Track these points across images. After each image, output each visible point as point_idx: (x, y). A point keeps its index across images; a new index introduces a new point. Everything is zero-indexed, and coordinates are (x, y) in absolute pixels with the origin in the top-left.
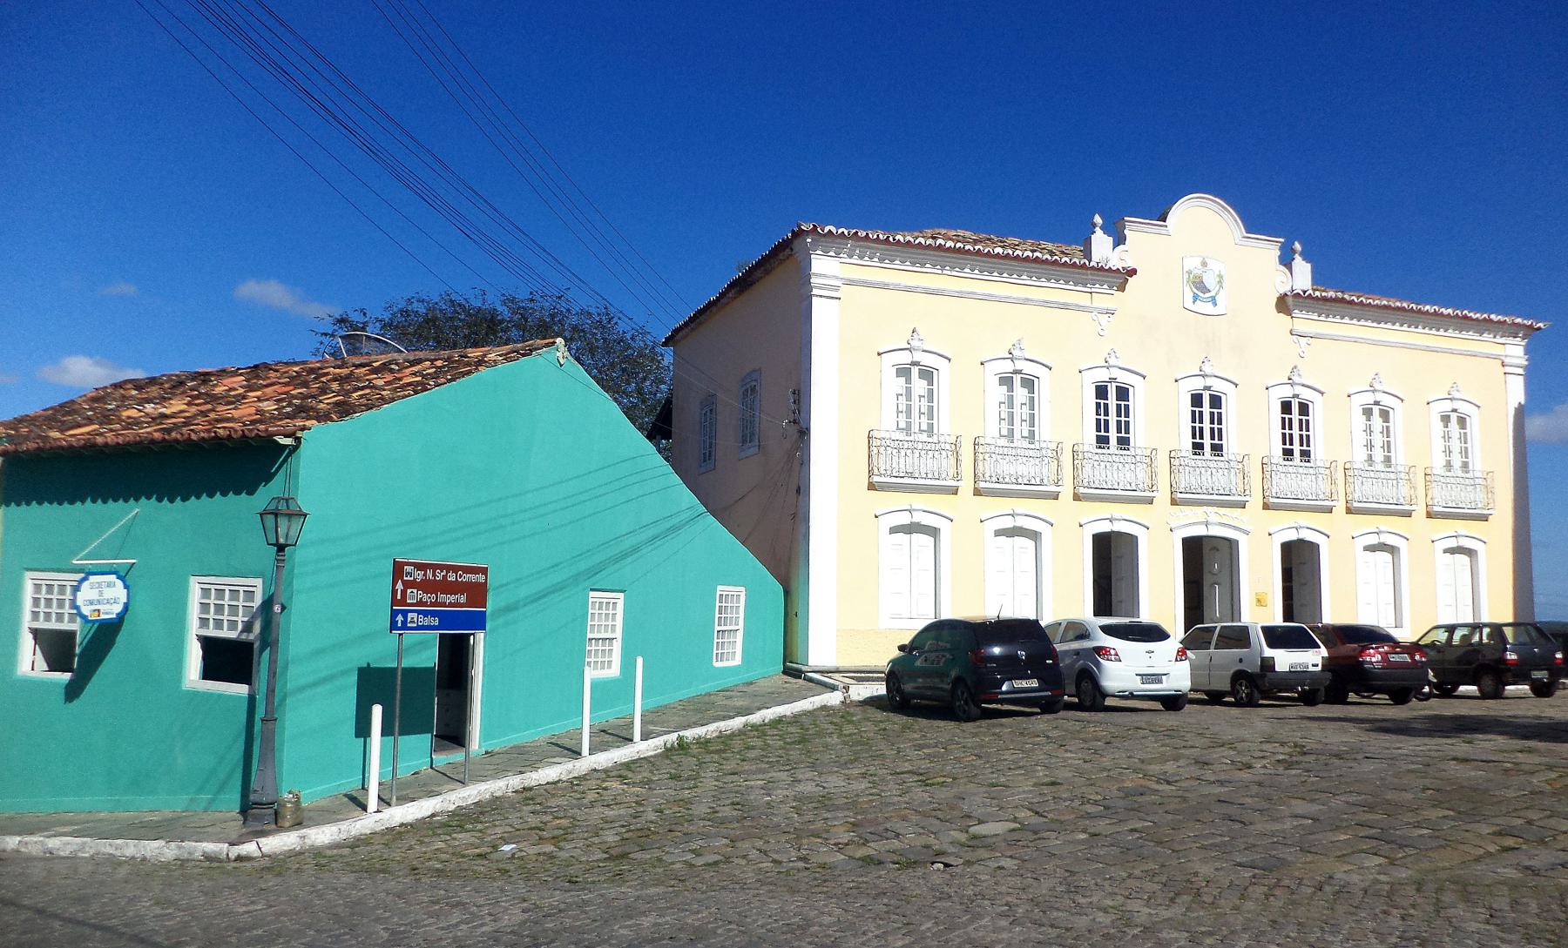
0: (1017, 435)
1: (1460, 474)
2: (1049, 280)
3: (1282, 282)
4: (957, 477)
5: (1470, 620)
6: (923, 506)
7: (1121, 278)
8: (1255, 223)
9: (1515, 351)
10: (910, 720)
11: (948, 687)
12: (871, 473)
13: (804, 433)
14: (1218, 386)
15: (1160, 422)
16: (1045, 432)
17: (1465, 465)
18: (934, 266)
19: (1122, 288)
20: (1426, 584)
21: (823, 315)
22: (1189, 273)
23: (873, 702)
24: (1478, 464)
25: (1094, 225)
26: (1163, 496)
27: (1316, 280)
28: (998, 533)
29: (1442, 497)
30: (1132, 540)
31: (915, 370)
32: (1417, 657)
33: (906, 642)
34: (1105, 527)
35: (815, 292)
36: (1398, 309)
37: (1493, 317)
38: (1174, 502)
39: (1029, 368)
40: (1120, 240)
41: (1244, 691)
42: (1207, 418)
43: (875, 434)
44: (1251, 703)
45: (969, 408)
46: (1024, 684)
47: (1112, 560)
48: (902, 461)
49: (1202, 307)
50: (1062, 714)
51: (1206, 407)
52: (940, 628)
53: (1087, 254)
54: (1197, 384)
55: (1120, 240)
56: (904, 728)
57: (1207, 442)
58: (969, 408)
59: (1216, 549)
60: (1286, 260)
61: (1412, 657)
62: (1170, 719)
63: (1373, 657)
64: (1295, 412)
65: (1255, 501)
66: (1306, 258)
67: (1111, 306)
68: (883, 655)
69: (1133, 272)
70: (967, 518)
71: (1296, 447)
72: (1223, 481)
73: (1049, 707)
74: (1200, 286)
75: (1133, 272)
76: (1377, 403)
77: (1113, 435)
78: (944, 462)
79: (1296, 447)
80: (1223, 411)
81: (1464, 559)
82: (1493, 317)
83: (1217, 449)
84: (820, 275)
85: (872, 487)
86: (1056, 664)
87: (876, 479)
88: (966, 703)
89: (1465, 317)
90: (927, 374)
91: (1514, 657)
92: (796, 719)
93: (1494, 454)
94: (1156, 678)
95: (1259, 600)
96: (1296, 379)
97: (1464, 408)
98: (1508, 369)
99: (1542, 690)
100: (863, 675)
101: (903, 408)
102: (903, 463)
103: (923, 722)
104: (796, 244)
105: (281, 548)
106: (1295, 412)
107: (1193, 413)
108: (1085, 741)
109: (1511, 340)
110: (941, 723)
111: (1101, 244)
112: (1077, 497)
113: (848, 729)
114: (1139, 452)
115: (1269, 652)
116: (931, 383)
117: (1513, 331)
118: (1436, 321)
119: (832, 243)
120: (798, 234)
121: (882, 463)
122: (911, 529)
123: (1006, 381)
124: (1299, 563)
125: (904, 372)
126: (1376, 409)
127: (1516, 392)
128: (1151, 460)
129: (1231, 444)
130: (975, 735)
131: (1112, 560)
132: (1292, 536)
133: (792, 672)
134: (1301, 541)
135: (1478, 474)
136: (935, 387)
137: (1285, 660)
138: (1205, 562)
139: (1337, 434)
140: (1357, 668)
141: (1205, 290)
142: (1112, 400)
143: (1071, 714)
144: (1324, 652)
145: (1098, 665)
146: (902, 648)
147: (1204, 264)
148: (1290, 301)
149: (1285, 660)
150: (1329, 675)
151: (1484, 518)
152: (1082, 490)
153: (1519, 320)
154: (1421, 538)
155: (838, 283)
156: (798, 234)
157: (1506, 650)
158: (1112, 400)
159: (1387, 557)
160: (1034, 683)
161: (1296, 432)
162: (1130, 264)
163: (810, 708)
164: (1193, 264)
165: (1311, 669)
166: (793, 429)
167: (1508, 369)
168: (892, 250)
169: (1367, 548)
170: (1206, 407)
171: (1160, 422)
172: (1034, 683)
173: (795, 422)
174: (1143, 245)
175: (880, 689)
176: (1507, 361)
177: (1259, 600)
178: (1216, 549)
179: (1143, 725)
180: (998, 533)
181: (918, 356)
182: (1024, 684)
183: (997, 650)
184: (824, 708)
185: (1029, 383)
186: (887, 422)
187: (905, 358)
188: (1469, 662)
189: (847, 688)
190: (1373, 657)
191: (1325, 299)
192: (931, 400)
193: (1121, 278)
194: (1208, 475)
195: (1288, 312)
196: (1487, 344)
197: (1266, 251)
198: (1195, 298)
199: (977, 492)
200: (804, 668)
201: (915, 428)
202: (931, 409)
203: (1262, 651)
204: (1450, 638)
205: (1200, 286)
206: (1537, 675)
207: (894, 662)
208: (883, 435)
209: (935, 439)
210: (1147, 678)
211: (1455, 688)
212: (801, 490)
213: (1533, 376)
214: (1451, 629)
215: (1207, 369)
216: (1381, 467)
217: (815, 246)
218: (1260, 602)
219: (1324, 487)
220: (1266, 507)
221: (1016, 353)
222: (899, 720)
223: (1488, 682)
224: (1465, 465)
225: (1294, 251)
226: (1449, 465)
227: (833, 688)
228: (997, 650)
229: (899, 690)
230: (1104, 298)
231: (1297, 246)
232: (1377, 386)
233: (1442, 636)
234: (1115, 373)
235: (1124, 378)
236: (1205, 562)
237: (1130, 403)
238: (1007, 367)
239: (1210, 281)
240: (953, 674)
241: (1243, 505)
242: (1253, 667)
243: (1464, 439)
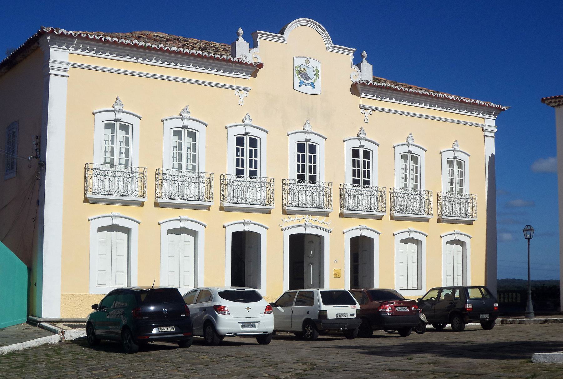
0: (184, 168)
1: (457, 196)
2: (207, 69)
3: (354, 75)
4: (144, 195)
5: (460, 285)
6: (120, 215)
7: (254, 69)
8: (339, 38)
9: (490, 122)
10: (94, 351)
11: (120, 331)
12: (86, 192)
13: (42, 164)
14: (314, 139)
15: (277, 163)
16: (203, 167)
17: (461, 191)
18: (132, 57)
19: (254, 75)
20: (431, 261)
21: (58, 90)
22: (298, 67)
23: (79, 341)
24: (468, 190)
25: (238, 35)
26: (277, 208)
27: (375, 72)
28: (170, 231)
29: (450, 209)
30: (256, 237)
31: (117, 125)
32: (413, 308)
33: (98, 303)
34: (240, 228)
35: (52, 72)
36: (423, 94)
37: (477, 101)
38: (284, 212)
39: (192, 125)
40: (254, 45)
41: (309, 331)
42: (247, 153)
43: (89, 166)
44: (313, 339)
45: (151, 150)
46: (166, 329)
47: (244, 248)
48: (107, 184)
49: (304, 88)
50: (192, 347)
51: (306, 151)
52: (117, 294)
53: (233, 54)
54: (301, 138)
55: (254, 45)
56: (91, 357)
57: (247, 169)
58: (151, 150)
59: (312, 242)
60: (357, 62)
61: (410, 309)
62: (263, 348)
63: (388, 309)
64: (361, 156)
65: (335, 211)
66: (369, 61)
67: (247, 86)
68: (85, 312)
69: (261, 66)
70: (149, 222)
71: (361, 176)
72: (316, 199)
73: (183, 343)
74: (303, 74)
75: (261, 66)
76: (455, 157)
77: (247, 169)
78: (135, 185)
79: (361, 176)
80: (371, 160)
81: (458, 247)
82: (477, 101)
83: (253, 174)
84: (56, 61)
85: (86, 200)
86: (188, 316)
87: (160, 200)
88: (130, 342)
89: (462, 101)
90: (125, 128)
91: (470, 306)
92: (25, 351)
93: (477, 184)
94: (251, 324)
95: (336, 273)
96: (362, 136)
97: (460, 156)
98: (486, 134)
99: (487, 325)
100: (74, 324)
101: (109, 149)
102: (107, 185)
103: (104, 353)
104: (41, 40)
105: (529, 239)
106: (361, 156)
107: (354, 161)
108: (193, 364)
109: (488, 116)
110: (114, 354)
111: (242, 46)
112: (222, 209)
113: (56, 359)
114: (263, 180)
115: (324, 307)
116: (194, 140)
117: (489, 111)
118: (446, 103)
119: (64, 41)
120: (42, 34)
121: (94, 185)
122: (113, 228)
123: (177, 133)
124: (361, 250)
125: (109, 126)
126: (410, 156)
127: (490, 148)
128: (382, 193)
129: (263, 171)
130: (130, 361)
131: (244, 248)
132: (357, 234)
133: (32, 322)
134: (363, 238)
135: (467, 196)
136: (197, 142)
137: (333, 311)
138: (303, 252)
139: (386, 173)
140: (380, 317)
141: (308, 78)
142: (248, 147)
143: (197, 348)
144: (358, 306)
145: (216, 317)
146: (94, 307)
147: (307, 62)
148: (359, 87)
149: (333, 311)
150: (360, 320)
151: (471, 223)
152: (225, 204)
153: (492, 104)
154: (435, 234)
155: (68, 67)
156: (42, 34)
157: (466, 303)
158: (248, 147)
159: (414, 246)
160: (173, 329)
161: (361, 169)
162: (260, 61)
163: (37, 345)
164: (300, 62)
165: (350, 317)
166: (35, 162)
167: (486, 134)
168: (103, 46)
169: (402, 241)
170: (306, 151)
171: (277, 163)
172: (173, 329)
173: (37, 157)
174: (268, 49)
175: (82, 333)
176: (486, 128)
177: (336, 273)
178: (312, 242)
179: (233, 354)
180: (170, 231)
181: (119, 116)
182: (166, 329)
183: (152, 308)
184: (46, 345)
185: (192, 135)
186: (98, 159)
187: (111, 116)
188: (448, 309)
189: (63, 332)
190: (388, 309)
191: (380, 87)
192: (194, 150)
193: (254, 69)
194: (244, 191)
195: (358, 94)
196: (474, 118)
197: (345, 57)
198: (301, 83)
199: (157, 205)
200: (39, 319)
201: (116, 162)
202: (194, 156)
203: (320, 306)
204: (439, 296)
205: (303, 74)
206: (483, 316)
207: (92, 315)
208: (165, 172)
209: (197, 175)
210: (246, 324)
211: (444, 325)
212: (40, 203)
213: (500, 138)
214: (440, 290)
215: (308, 128)
216: (411, 191)
217: (52, 42)
218: (336, 275)
219: (264, 195)
220: (342, 215)
221: (184, 115)
222: (89, 352)
223: (456, 321)
224: (461, 191)
225: (362, 57)
226: (452, 190)
227: (54, 332)
228: (152, 308)
229: (93, 334)
230: (242, 80)
231: (365, 53)
232: (410, 142)
233: (435, 294)
234: (249, 129)
235: (254, 133)
236: (303, 252)
237: (258, 149)
238: (179, 124)
239: (310, 73)
240: (124, 322)
241: (327, 214)
242: (314, 316)
243: (461, 174)
